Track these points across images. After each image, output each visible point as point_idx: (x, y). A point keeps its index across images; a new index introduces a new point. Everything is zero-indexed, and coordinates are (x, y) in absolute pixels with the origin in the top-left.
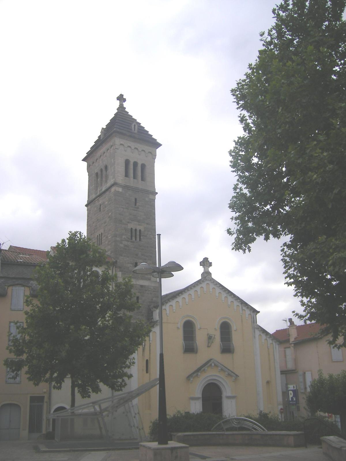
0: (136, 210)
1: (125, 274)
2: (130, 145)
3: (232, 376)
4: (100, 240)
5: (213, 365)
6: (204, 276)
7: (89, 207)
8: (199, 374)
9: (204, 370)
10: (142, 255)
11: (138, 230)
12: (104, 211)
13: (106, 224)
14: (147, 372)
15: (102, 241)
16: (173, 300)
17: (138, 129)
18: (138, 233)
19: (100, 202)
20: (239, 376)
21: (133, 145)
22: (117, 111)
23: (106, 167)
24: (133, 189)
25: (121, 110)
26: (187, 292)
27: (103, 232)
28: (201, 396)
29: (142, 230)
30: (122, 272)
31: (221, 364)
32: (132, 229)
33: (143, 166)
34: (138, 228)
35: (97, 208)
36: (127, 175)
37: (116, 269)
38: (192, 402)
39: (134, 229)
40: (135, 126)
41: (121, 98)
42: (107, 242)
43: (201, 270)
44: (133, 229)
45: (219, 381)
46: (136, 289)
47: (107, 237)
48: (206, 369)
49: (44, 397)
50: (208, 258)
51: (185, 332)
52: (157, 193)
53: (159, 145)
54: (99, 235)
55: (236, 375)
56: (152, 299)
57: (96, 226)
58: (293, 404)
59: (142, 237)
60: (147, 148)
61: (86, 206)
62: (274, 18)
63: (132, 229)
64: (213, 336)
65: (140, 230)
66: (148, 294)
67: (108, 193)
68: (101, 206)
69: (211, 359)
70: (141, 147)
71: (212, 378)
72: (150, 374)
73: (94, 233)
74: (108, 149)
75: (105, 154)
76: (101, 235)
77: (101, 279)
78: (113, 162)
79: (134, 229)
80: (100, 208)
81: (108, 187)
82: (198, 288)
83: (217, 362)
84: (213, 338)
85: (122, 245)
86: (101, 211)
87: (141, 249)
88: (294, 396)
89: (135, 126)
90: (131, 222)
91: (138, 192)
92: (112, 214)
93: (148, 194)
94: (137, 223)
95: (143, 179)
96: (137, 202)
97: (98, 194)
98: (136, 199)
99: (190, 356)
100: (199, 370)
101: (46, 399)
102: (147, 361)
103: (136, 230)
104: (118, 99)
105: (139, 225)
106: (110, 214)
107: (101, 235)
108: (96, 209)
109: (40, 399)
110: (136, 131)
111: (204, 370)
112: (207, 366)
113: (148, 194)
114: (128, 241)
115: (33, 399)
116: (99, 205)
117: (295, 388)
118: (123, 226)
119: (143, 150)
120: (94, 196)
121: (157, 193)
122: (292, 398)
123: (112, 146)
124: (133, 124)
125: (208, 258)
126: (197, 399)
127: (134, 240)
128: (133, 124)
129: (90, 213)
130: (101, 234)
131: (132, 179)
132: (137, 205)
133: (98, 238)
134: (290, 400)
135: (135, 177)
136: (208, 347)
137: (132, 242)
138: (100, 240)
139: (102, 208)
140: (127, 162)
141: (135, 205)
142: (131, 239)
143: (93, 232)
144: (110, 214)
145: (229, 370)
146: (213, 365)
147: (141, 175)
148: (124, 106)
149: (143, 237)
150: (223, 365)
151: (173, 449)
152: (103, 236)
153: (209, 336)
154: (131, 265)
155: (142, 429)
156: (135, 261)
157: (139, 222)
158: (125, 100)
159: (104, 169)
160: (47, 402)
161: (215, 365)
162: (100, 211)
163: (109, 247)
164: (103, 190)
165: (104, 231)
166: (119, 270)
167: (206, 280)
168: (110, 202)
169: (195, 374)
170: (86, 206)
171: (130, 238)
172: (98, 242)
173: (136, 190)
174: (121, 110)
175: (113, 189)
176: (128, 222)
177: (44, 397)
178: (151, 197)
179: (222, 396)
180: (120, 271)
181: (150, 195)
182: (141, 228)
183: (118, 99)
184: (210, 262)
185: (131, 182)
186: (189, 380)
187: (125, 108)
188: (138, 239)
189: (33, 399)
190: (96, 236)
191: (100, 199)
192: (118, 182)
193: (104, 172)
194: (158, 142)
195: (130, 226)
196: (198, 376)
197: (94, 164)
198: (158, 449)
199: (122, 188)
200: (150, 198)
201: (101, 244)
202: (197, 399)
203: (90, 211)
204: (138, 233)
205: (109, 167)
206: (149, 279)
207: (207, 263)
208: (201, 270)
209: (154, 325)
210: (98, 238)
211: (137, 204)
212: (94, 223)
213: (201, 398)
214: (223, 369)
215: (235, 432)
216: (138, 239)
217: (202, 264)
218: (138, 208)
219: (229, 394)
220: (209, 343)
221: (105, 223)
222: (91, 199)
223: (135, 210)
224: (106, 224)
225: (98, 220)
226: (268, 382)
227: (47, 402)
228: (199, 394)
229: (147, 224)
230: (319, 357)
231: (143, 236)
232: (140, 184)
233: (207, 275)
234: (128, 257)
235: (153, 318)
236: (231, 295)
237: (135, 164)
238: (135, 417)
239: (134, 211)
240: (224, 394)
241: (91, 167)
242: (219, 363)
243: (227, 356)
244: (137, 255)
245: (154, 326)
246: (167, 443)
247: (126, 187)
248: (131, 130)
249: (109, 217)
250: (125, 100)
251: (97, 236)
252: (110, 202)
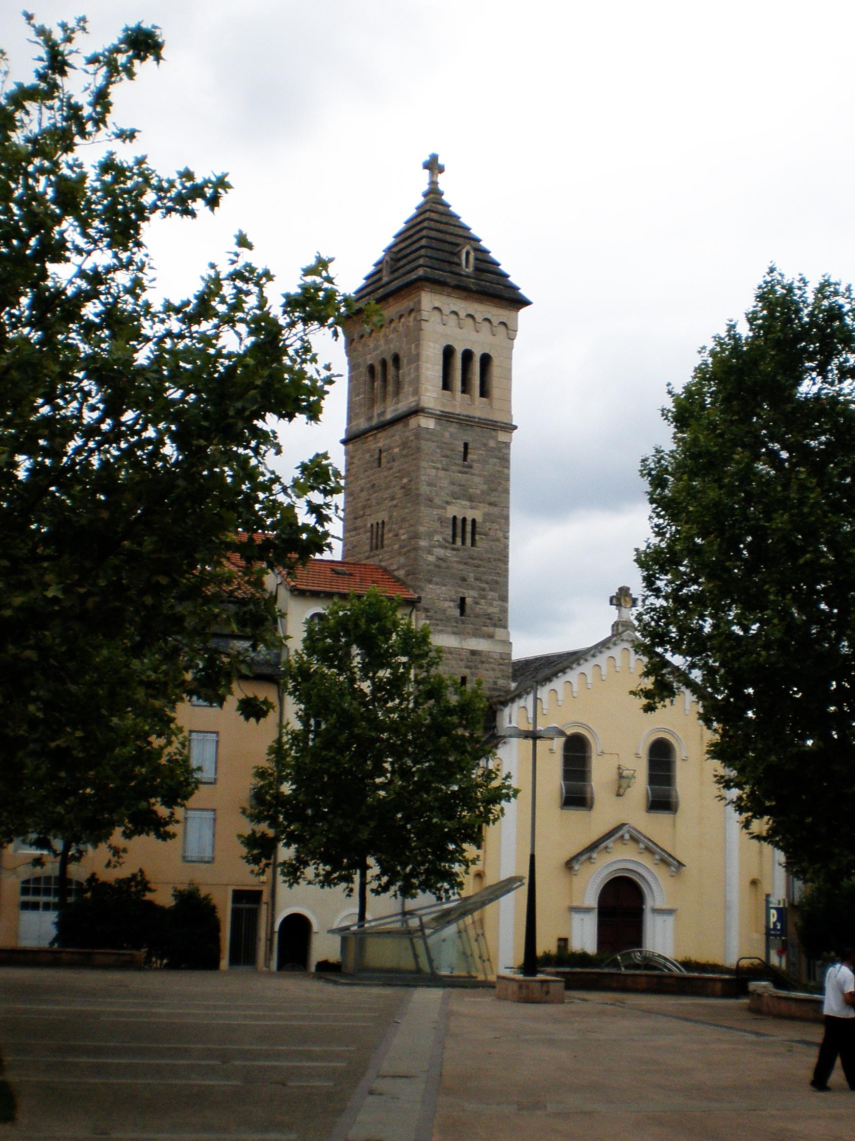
0: (466, 473)
1: (437, 625)
4: (380, 538)
5: (627, 836)
6: (617, 630)
7: (350, 446)
8: (595, 855)
9: (606, 848)
10: (477, 579)
13: (395, 502)
15: (385, 542)
16: (542, 686)
17: (476, 259)
18: (469, 528)
19: (380, 445)
20: (684, 866)
21: (463, 307)
23: (396, 359)
25: (433, 194)
27: (386, 520)
28: (596, 906)
29: (479, 520)
31: (645, 837)
32: (455, 518)
33: (486, 360)
34: (470, 515)
35: (372, 456)
36: (447, 385)
38: (576, 917)
39: (460, 517)
40: (468, 253)
41: (433, 166)
42: (396, 547)
45: (639, 874)
46: (462, 660)
47: (396, 535)
48: (611, 845)
50: (628, 589)
52: (515, 428)
53: (523, 302)
54: (378, 524)
55: (679, 863)
56: (495, 683)
57: (368, 500)
58: (775, 935)
59: (477, 537)
60: (497, 313)
61: (344, 442)
62: (632, 696)
63: (455, 518)
66: (487, 670)
67: (400, 426)
69: (623, 825)
70: (481, 310)
72: (485, 852)
73: (363, 516)
75: (393, 325)
76: (380, 526)
77: (105, 206)
78: (414, 352)
79: (460, 517)
80: (380, 459)
81: (400, 411)
82: (602, 659)
83: (637, 831)
85: (431, 559)
86: (383, 466)
88: (779, 919)
89: (468, 253)
91: (472, 426)
92: (410, 481)
95: (484, 392)
96: (469, 450)
97: (375, 422)
98: (466, 445)
99: (575, 815)
100: (593, 847)
101: (265, 897)
103: (464, 520)
105: (472, 508)
107: (380, 526)
108: (368, 456)
109: (254, 896)
110: (470, 270)
111: (606, 848)
114: (446, 548)
115: (239, 896)
116: (377, 451)
117: (781, 906)
120: (362, 424)
121: (515, 428)
122: (775, 923)
123: (412, 311)
124: (464, 251)
125: (628, 589)
126: (587, 910)
128: (464, 251)
129: (353, 463)
130: (380, 522)
133: (375, 530)
134: (772, 927)
135: (466, 389)
136: (619, 795)
137: (454, 549)
138: (380, 538)
139: (383, 460)
140: (448, 352)
141: (465, 459)
142: (454, 542)
143: (362, 513)
146: (627, 836)
150: (650, 840)
151: (543, 982)
152: (386, 529)
154: (452, 604)
156: (461, 595)
159: (390, 363)
160: (267, 903)
162: (380, 465)
163: (402, 560)
164: (389, 416)
165: (391, 518)
166: (424, 616)
167: (622, 640)
168: (405, 452)
169: (584, 857)
170: (344, 442)
171: (451, 540)
172: (374, 541)
173: (466, 422)
174: (433, 194)
175: (413, 422)
176: (448, 503)
177: (259, 893)
178: (502, 437)
181: (499, 432)
184: (634, 596)
185: (459, 403)
187: (442, 194)
189: (239, 896)
190: (369, 525)
191: (379, 435)
192: (426, 406)
193: (391, 370)
195: (452, 511)
196: (593, 861)
197: (363, 339)
198: (525, 981)
201: (382, 547)
202: (587, 910)
203: (353, 457)
204: (469, 528)
205: (404, 361)
206: (491, 636)
207: (627, 599)
209: (498, 744)
210: (375, 530)
211: (470, 457)
212: (362, 490)
213: (596, 910)
214: (651, 849)
215: (638, 972)
217: (614, 601)
218: (470, 467)
219: (659, 905)
220: (620, 787)
221: (393, 498)
222: (355, 430)
224: (395, 502)
225: (373, 486)
226: (754, 883)
227: (267, 903)
228: (591, 900)
229: (490, 504)
230: (464, 953)
232: (477, 408)
234: (445, 585)
235: (495, 727)
237: (468, 356)
241: (354, 344)
242: (639, 832)
243: (663, 817)
245: (500, 745)
247: (444, 418)
248: (459, 265)
249: (402, 488)
251: (372, 525)
252: (405, 452)
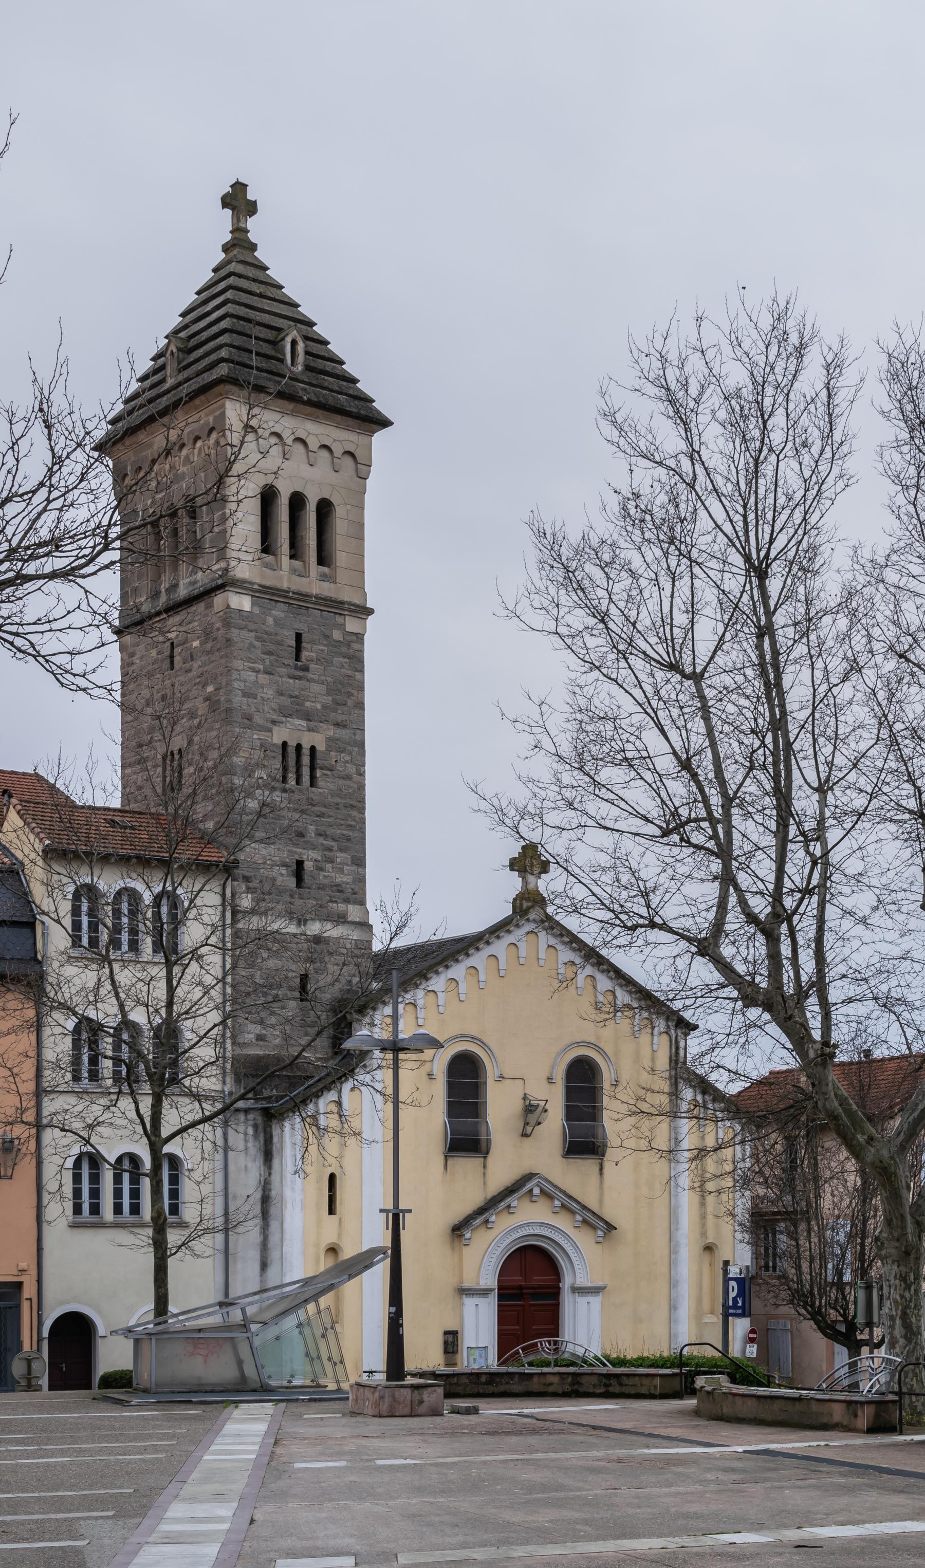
2: (278, 429)
3: (594, 1228)
5: (536, 1191)
8: (493, 1218)
11: (306, 747)
12: (188, 671)
14: (332, 1211)
18: (306, 760)
22: (223, 255)
24: (291, 598)
26: (462, 960)
29: (321, 747)
30: (252, 893)
32: (285, 744)
33: (325, 508)
36: (267, 546)
37: (235, 883)
39: (292, 744)
40: (294, 343)
43: (513, 884)
44: (290, 743)
49: (19, 1285)
51: (452, 1088)
59: (319, 773)
64: (542, 1103)
65: (313, 749)
67: (200, 607)
68: (175, 650)
71: (532, 1232)
74: (197, 438)
79: (292, 744)
80: (172, 657)
84: (540, 1109)
87: (318, 816)
90: (284, 719)
93: (341, 614)
94: (304, 723)
95: (323, 559)
96: (304, 645)
98: (299, 637)
99: (466, 1165)
101: (29, 1291)
102: (332, 1178)
103: (299, 747)
104: (227, 202)
106: (210, 689)
108: (154, 653)
111: (509, 1206)
112: (516, 1195)
113: (341, 614)
118: (255, 736)
119: (324, 447)
124: (289, 339)
127: (294, 783)
128: (289, 339)
129: (133, 664)
131: (285, 560)
132: (303, 659)
139: (177, 659)
140: (268, 497)
141: (298, 658)
142: (284, 780)
144: (210, 689)
145: (584, 1207)
146: (536, 1191)
147: (315, 543)
148: (252, 237)
149: (325, 772)
153: (527, 1102)
155: (342, 1362)
156: (297, 857)
157: (310, 720)
158: (252, 208)
161: (542, 1191)
164: (183, 592)
165: (190, 742)
168: (208, 646)
171: (279, 777)
176: (274, 722)
179: (561, 1285)
180: (249, 890)
182: (318, 740)
183: (227, 202)
186: (461, 1236)
188: (306, 779)
194: (377, 410)
195: (278, 736)
196: (490, 1225)
199: (252, 596)
200: (347, 630)
204: (306, 760)
208: (513, 884)
211: (305, 654)
216: (306, 779)
218: (306, 669)
219: (582, 1280)
223: (294, 677)
228: (489, 1279)
231: (321, 768)
233: (530, 904)
236: (609, 971)
237: (297, 501)
238: (323, 1336)
239: (291, 681)
240: (567, 1281)
244: (301, 835)
246: (404, 1380)
248: (282, 361)
249: (207, 699)
250: (252, 208)
252: (208, 646)
